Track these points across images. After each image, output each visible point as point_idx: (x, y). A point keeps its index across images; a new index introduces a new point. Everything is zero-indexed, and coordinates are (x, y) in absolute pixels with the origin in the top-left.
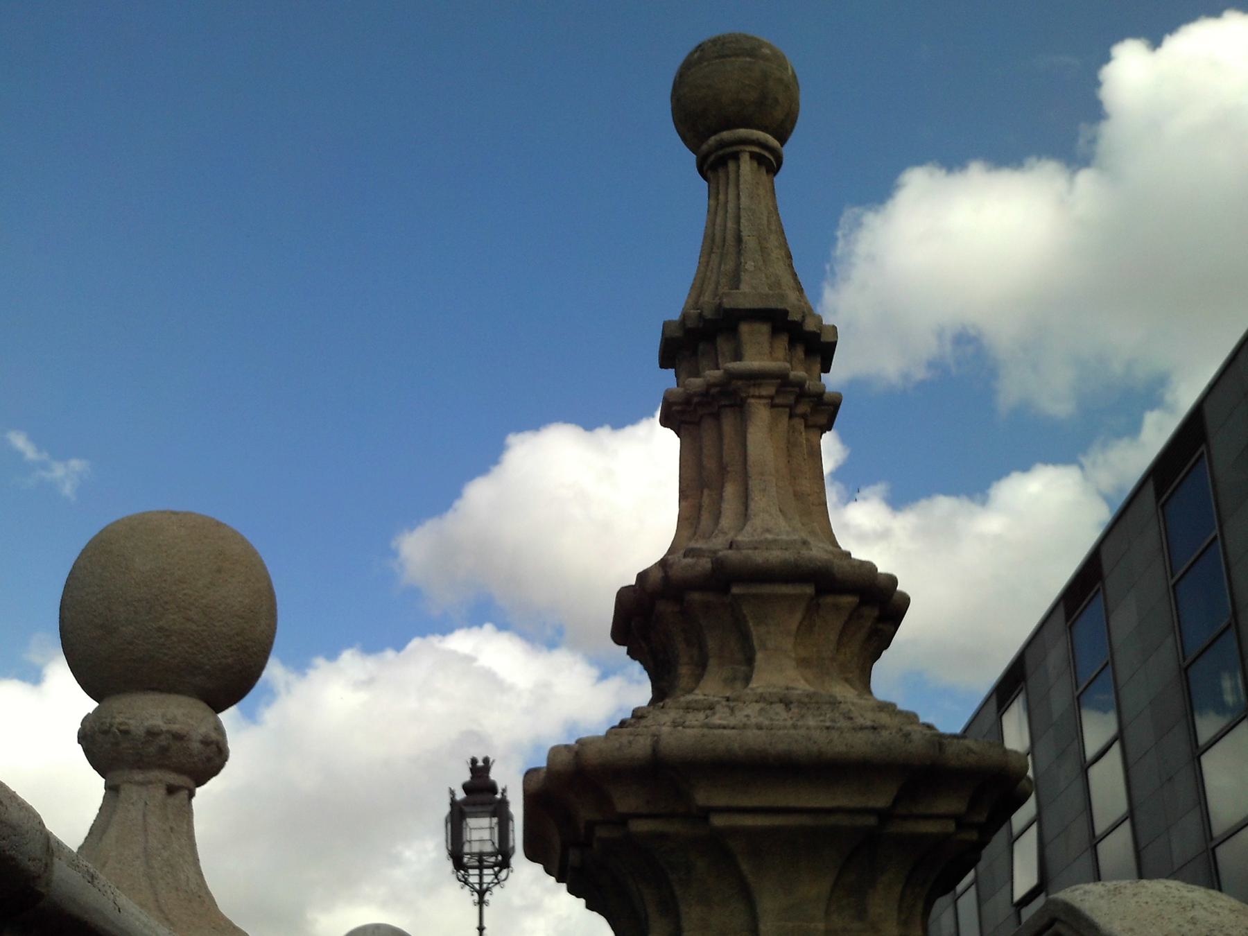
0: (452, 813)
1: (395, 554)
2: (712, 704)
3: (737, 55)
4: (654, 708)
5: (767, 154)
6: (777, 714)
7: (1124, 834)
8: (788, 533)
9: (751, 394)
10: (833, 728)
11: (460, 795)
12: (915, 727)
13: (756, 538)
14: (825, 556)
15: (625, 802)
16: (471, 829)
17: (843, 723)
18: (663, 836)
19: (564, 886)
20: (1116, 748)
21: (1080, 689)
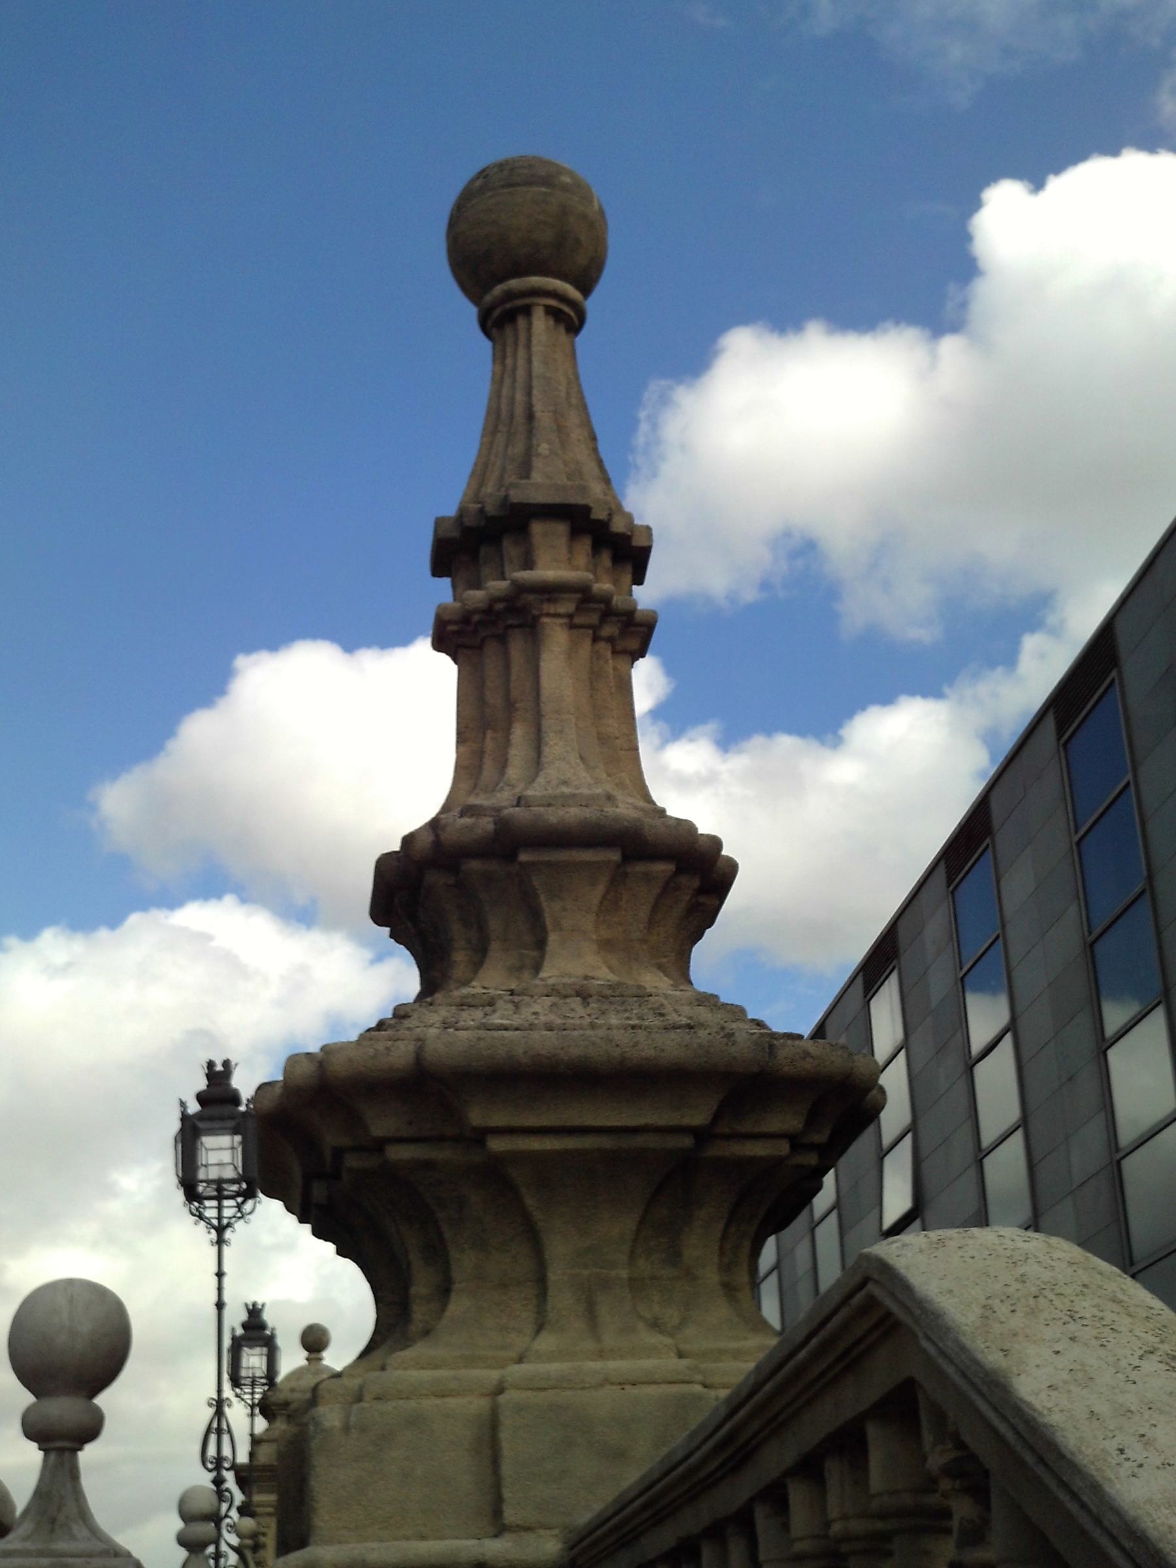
0: (182, 1130)
1: (93, 808)
2: (493, 998)
3: (529, 183)
4: (420, 1006)
5: (566, 309)
6: (573, 1010)
7: (1016, 1144)
8: (589, 786)
9: (545, 611)
10: (640, 1027)
11: (194, 1107)
12: (741, 1025)
13: (550, 791)
14: (633, 814)
15: (381, 1124)
16: (206, 1149)
17: (652, 1021)
18: (429, 1165)
19: (307, 1228)
20: (1008, 1039)
21: (965, 969)
